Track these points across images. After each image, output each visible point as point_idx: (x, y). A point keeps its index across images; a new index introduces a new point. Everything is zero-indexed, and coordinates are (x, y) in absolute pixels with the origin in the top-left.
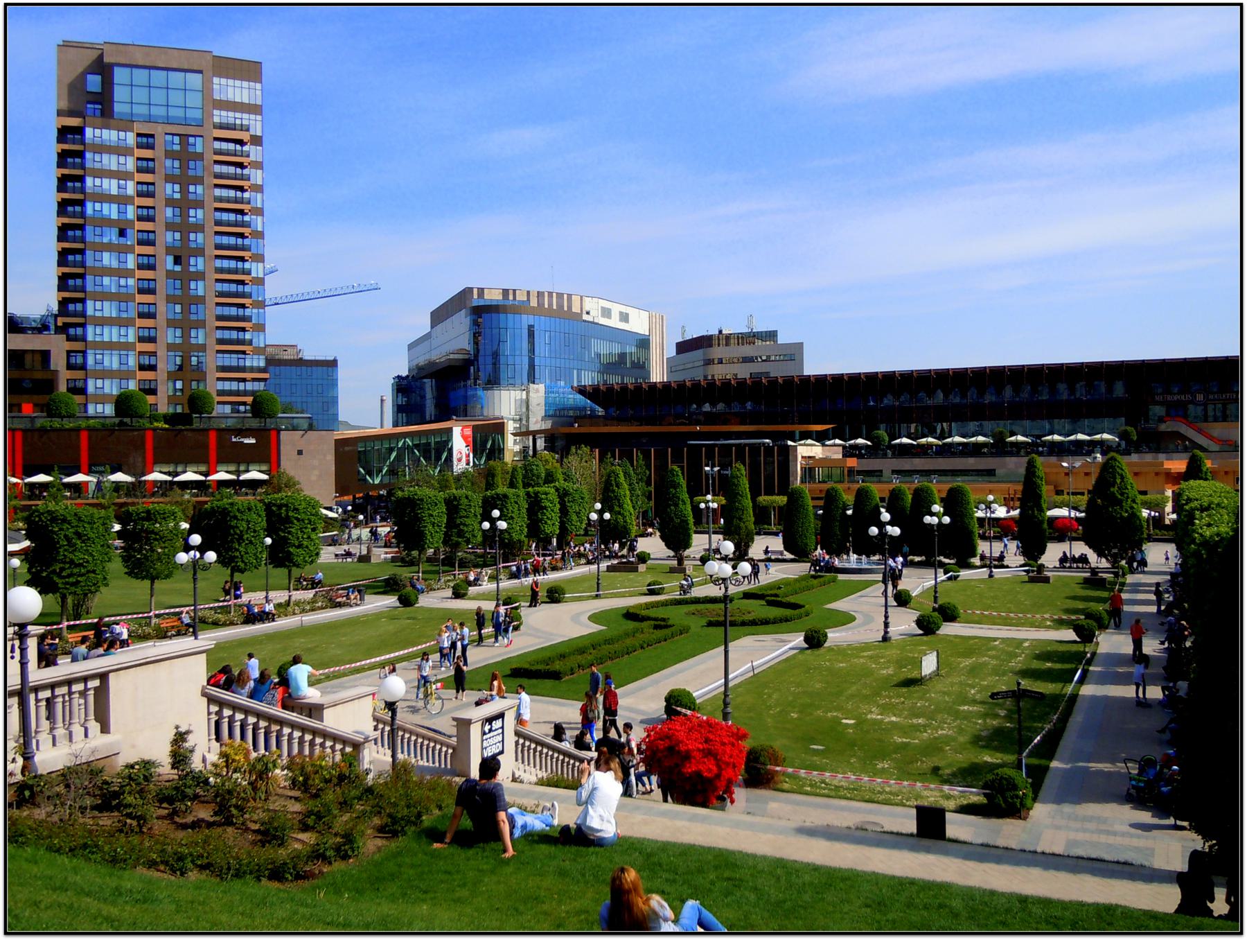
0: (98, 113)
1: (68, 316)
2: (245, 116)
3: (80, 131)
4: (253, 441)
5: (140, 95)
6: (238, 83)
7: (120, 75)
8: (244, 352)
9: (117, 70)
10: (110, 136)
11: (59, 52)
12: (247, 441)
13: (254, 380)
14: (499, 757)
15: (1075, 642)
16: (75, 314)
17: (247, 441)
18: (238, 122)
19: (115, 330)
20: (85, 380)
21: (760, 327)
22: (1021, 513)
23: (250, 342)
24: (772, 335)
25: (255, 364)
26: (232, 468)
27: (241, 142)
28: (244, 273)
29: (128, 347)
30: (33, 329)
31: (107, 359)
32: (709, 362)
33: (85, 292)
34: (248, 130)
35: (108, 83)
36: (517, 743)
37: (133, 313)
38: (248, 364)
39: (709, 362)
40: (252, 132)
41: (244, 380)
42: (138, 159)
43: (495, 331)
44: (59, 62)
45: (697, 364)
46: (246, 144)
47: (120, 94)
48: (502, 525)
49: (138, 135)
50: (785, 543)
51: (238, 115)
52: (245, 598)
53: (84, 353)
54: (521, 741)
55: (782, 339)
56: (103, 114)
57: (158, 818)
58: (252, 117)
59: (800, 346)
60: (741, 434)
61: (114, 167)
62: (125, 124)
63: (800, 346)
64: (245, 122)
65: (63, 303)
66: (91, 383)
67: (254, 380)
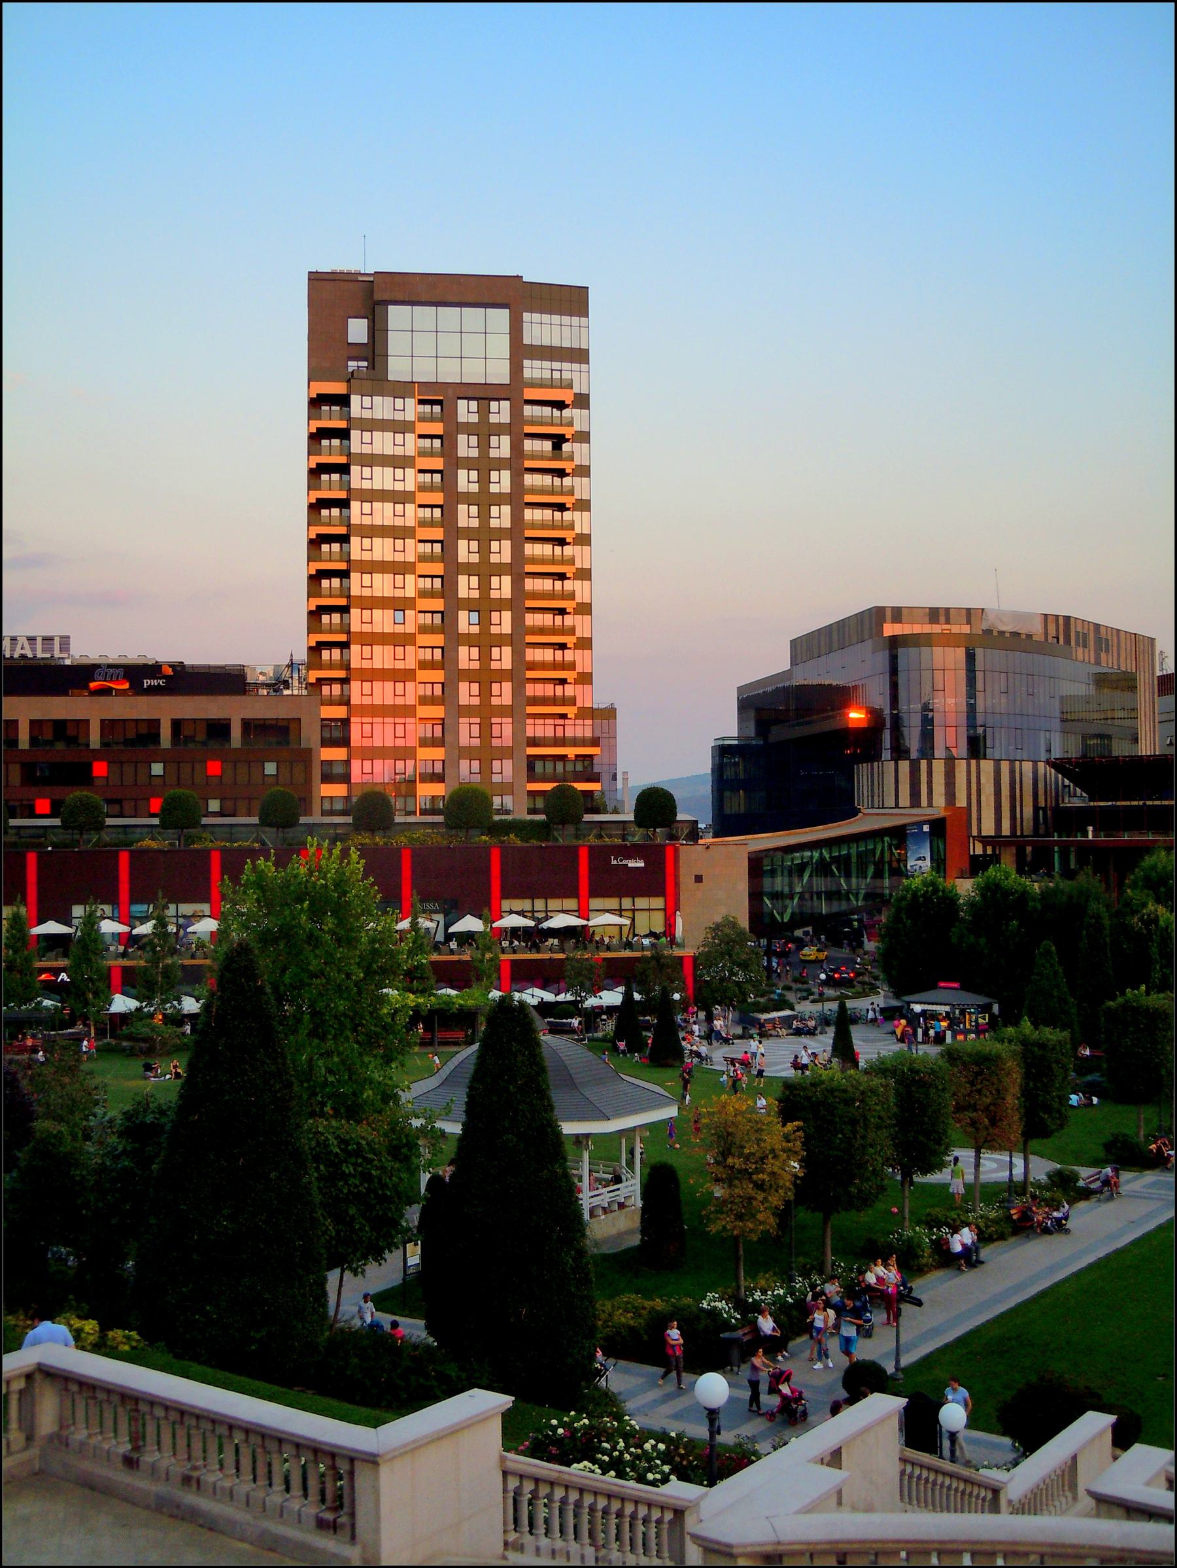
1: (320, 667)
3: (343, 401)
4: (641, 864)
5: (425, 344)
8: (564, 716)
9: (727, 811)
12: (632, 864)
14: (843, 1394)
17: (632, 864)
18: (556, 375)
20: (348, 763)
22: (194, 1089)
25: (579, 734)
27: (560, 405)
29: (407, 711)
31: (377, 729)
33: (349, 632)
36: (903, 1473)
38: (569, 733)
42: (420, 436)
47: (396, 343)
48: (554, 1422)
51: (556, 365)
54: (909, 1469)
58: (576, 366)
65: (316, 650)
66: (356, 765)
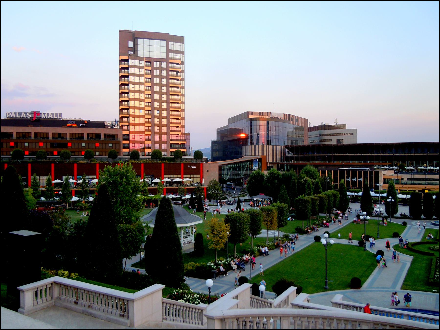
2: (179, 55)
3: (127, 61)
4: (195, 167)
6: (175, 43)
7: (140, 41)
8: (178, 135)
12: (193, 167)
16: (125, 122)
17: (193, 167)
18: (177, 57)
19: (138, 127)
20: (129, 144)
21: (340, 123)
24: (344, 126)
25: (182, 139)
26: (169, 176)
31: (136, 137)
34: (180, 60)
35: (135, 45)
36: (251, 300)
38: (179, 138)
40: (181, 61)
43: (258, 127)
45: (316, 136)
50: (361, 207)
55: (348, 128)
59: (355, 130)
60: (356, 166)
62: (141, 59)
63: (355, 130)
64: (179, 57)
66: (131, 145)
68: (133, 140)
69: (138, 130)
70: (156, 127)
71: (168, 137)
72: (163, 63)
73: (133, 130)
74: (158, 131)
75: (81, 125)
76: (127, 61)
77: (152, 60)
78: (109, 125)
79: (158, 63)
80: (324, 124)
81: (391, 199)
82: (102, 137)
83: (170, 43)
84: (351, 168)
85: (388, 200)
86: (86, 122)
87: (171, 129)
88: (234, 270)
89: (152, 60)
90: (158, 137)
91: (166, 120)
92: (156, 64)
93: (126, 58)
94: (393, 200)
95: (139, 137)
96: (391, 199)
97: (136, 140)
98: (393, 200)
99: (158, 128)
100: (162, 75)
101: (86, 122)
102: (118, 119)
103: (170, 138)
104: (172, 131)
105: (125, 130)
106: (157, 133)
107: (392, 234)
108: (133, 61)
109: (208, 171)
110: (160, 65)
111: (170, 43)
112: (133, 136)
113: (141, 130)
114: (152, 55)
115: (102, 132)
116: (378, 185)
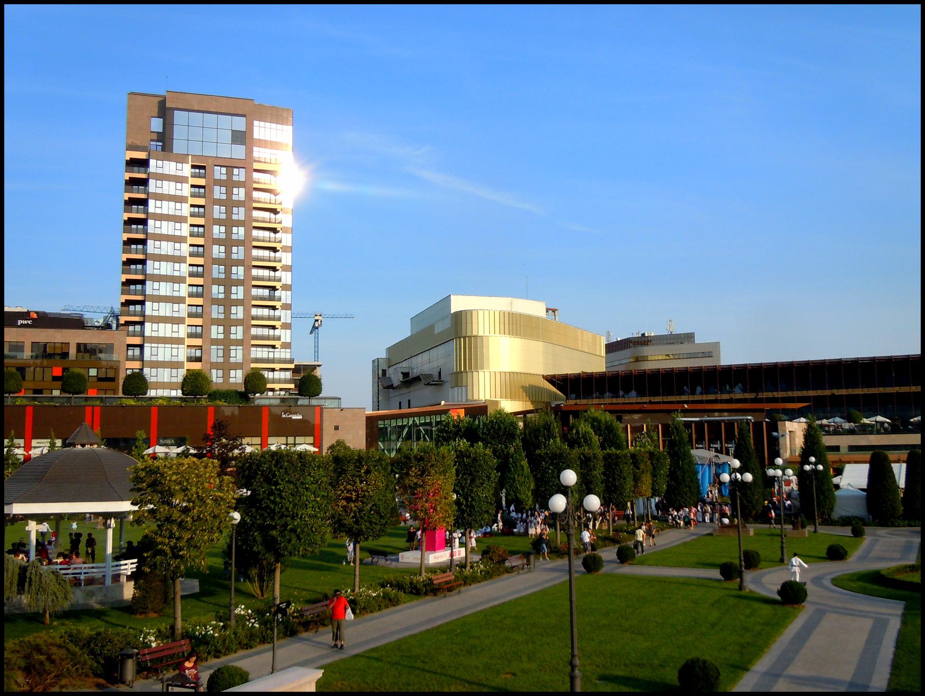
0: (160, 148)
3: (144, 163)
7: (179, 117)
8: (274, 347)
10: (170, 167)
11: (129, 99)
12: (294, 417)
13: (281, 369)
15: (718, 580)
23: (279, 338)
24: (690, 337)
28: (274, 280)
30: (98, 327)
32: (638, 360)
35: (168, 125)
37: (184, 314)
38: (277, 355)
39: (638, 360)
41: (273, 370)
44: (129, 107)
46: (278, 232)
49: (193, 167)
52: (640, 539)
53: (141, 347)
55: (697, 340)
56: (163, 149)
57: (262, 595)
59: (717, 345)
61: (172, 192)
62: (181, 159)
63: (717, 345)
67: (281, 369)
68: (154, 358)
69: (168, 335)
70: (214, 328)
71: (246, 353)
72: (236, 171)
73: (154, 334)
74: (221, 336)
75: (20, 322)
76: (144, 163)
77: (210, 161)
78: (96, 324)
79: (224, 170)
80: (643, 335)
81: (816, 464)
82: (73, 351)
83: (256, 123)
84: (707, 418)
85: (807, 467)
86: (35, 316)
87: (254, 331)
88: (114, 608)
89: (210, 161)
90: (221, 353)
91: (240, 309)
92: (220, 173)
93: (142, 155)
94: (820, 467)
95: (168, 351)
96: (816, 464)
97: (161, 358)
98: (820, 467)
99: (221, 329)
100: (235, 217)
101: (35, 316)
102: (117, 308)
103: (253, 356)
104: (256, 337)
105: (134, 335)
106: (216, 342)
107: (824, 553)
108: (160, 163)
109: (336, 428)
110: (230, 174)
111: (256, 123)
112: (154, 353)
113: (175, 335)
114: (210, 152)
115: (72, 338)
116: (775, 434)
